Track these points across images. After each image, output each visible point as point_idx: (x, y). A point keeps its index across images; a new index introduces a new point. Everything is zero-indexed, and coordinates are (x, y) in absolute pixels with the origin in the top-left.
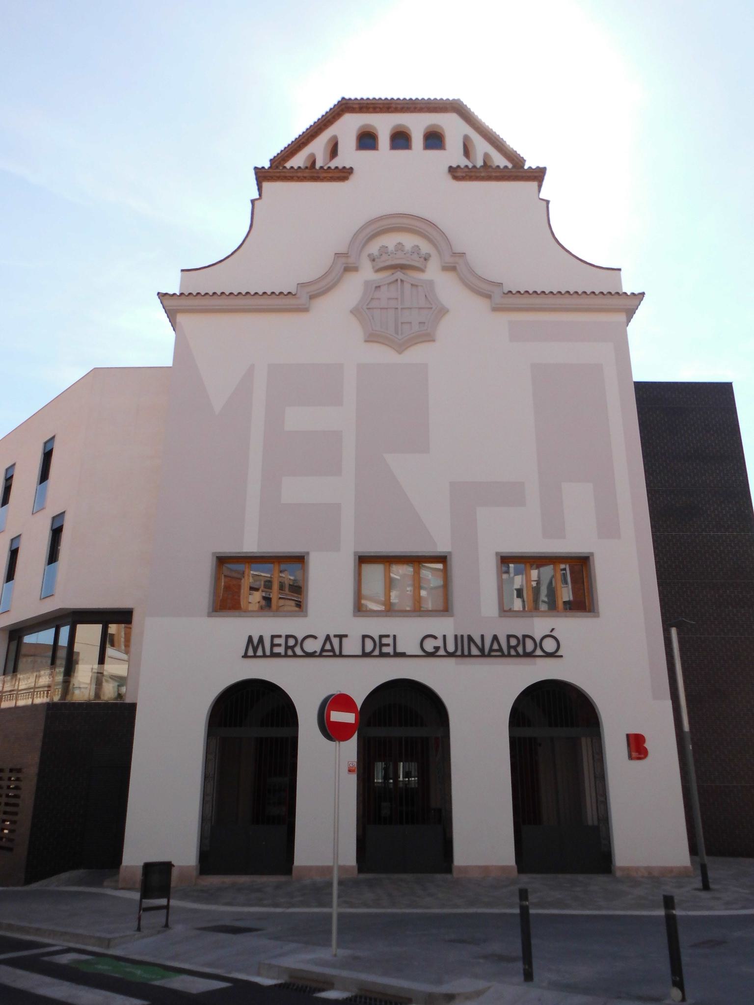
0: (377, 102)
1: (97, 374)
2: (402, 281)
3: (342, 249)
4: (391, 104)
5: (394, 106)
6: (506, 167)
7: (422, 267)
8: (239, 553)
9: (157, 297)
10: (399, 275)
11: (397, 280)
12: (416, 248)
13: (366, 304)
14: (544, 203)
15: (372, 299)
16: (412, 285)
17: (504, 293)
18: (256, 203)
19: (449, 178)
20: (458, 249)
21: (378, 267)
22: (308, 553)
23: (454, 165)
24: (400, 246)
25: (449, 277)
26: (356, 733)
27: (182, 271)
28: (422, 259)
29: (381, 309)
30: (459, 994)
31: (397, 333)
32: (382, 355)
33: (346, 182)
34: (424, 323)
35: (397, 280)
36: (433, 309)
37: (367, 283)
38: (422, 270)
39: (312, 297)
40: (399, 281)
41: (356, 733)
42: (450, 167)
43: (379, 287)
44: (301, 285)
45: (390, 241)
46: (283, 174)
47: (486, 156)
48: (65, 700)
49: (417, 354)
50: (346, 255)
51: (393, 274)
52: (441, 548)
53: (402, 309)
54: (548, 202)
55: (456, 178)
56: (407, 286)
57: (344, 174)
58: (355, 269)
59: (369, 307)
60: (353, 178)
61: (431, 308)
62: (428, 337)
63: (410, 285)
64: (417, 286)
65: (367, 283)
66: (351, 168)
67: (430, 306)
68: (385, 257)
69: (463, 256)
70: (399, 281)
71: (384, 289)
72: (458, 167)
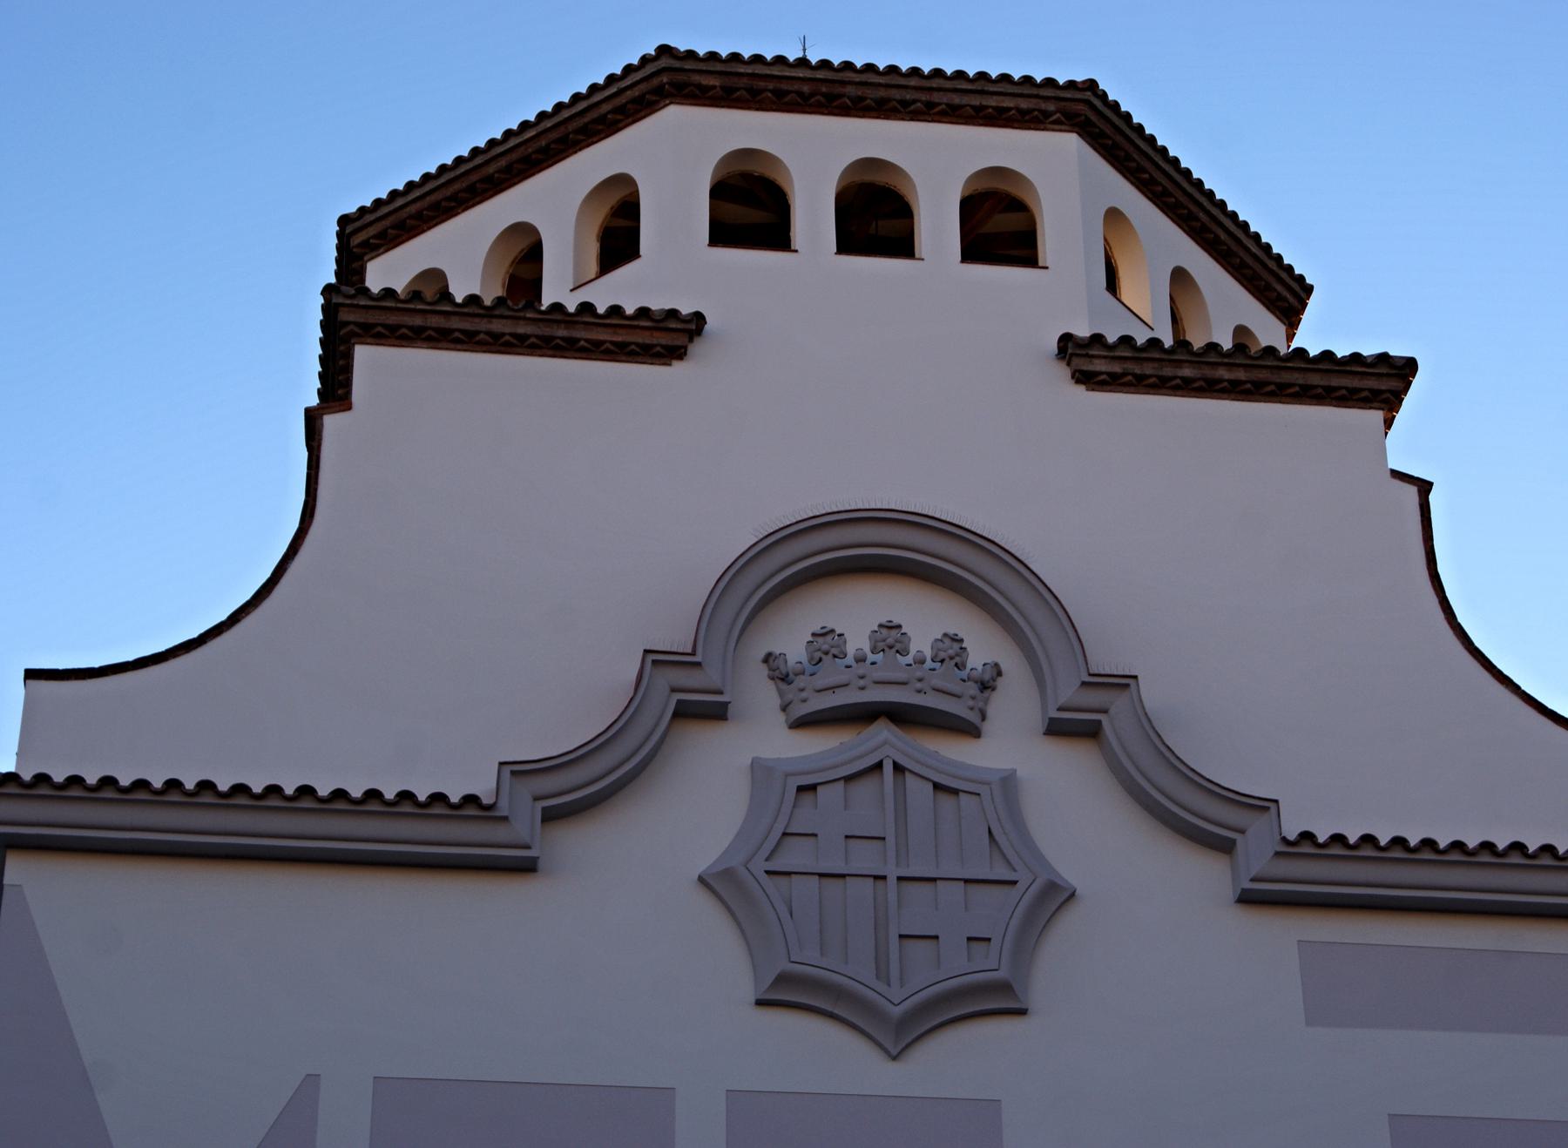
2: (898, 768)
3: (676, 637)
7: (973, 717)
10: (882, 738)
11: (879, 766)
12: (951, 650)
14: (1412, 492)
15: (785, 834)
16: (937, 787)
17: (1285, 840)
20: (1106, 661)
23: (1083, 331)
24: (826, 644)
25: (1073, 761)
27: (31, 675)
28: (972, 689)
30: (883, 782)
31: (882, 973)
33: (678, 367)
34: (989, 940)
37: (760, 770)
38: (969, 730)
39: (552, 816)
40: (888, 768)
42: (1066, 339)
43: (812, 788)
44: (517, 771)
46: (435, 321)
47: (1241, 332)
50: (686, 661)
51: (859, 734)
53: (900, 879)
54: (1425, 487)
55: (1085, 379)
58: (717, 713)
59: (771, 866)
61: (1014, 883)
63: (930, 786)
64: (955, 792)
65: (760, 770)
66: (699, 318)
67: (1002, 873)
68: (831, 673)
69: (1127, 686)
70: (888, 768)
72: (1097, 339)
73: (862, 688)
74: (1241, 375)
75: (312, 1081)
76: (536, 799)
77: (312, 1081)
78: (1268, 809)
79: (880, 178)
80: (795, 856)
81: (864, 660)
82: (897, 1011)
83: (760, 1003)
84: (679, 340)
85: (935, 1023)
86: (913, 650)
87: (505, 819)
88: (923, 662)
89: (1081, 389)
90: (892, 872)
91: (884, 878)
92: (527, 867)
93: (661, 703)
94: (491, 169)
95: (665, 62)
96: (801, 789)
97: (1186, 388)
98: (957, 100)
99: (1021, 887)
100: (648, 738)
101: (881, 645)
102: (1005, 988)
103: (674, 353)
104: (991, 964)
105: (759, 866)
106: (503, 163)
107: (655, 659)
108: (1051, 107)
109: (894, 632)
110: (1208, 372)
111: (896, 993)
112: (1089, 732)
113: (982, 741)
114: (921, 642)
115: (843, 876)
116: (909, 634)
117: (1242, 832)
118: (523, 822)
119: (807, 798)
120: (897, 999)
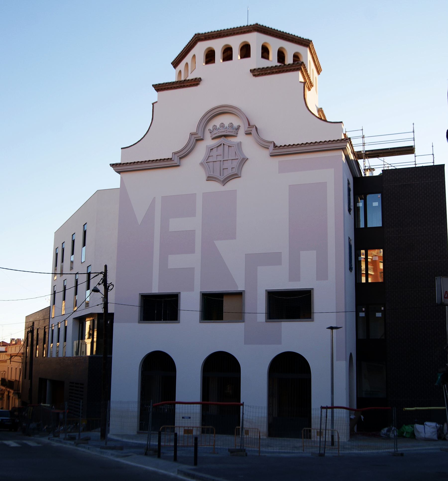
0: (213, 33)
1: (99, 192)
3: (194, 130)
4: (221, 33)
5: (222, 34)
6: (280, 66)
8: (150, 293)
9: (110, 166)
10: (222, 140)
11: (221, 144)
12: (231, 125)
13: (206, 160)
15: (209, 156)
18: (155, 104)
19: (251, 75)
21: (212, 137)
22: (180, 293)
24: (222, 125)
26: (6, 442)
27: (122, 148)
28: (234, 130)
29: (213, 162)
32: (215, 186)
33: (198, 86)
35: (221, 144)
36: (220, 176)
39: (181, 158)
40: (222, 144)
41: (6, 442)
44: (175, 153)
45: (217, 122)
48: (360, 199)
49: (232, 185)
52: (240, 288)
53: (223, 161)
55: (255, 75)
56: (226, 147)
57: (196, 82)
58: (202, 140)
59: (207, 161)
60: (202, 83)
62: (236, 176)
67: (237, 158)
70: (222, 144)
71: (215, 150)
73: (219, 133)
74: (277, 70)
75: (155, 198)
76: (178, 157)
77: (155, 198)
78: (272, 143)
79: (228, 47)
80: (211, 159)
81: (219, 129)
82: (222, 180)
83: (207, 180)
84: (197, 83)
85: (228, 180)
86: (225, 126)
87: (173, 160)
88: (227, 128)
89: (254, 77)
90: (222, 160)
91: (221, 161)
92: (178, 166)
93: (193, 140)
94: (183, 54)
95: (196, 36)
96: (211, 149)
97: (269, 74)
98: (238, 31)
99: (239, 159)
100: (192, 145)
101: (221, 126)
102: (236, 174)
103: (197, 84)
104: (235, 171)
105: (205, 161)
106: (184, 53)
107: (192, 134)
108: (252, 29)
109: (222, 124)
110: (272, 71)
111: (222, 177)
112: (250, 134)
113: (237, 137)
114: (226, 125)
115: (216, 161)
116: (224, 123)
117: (269, 146)
118: (176, 160)
119: (212, 150)
120: (222, 178)
